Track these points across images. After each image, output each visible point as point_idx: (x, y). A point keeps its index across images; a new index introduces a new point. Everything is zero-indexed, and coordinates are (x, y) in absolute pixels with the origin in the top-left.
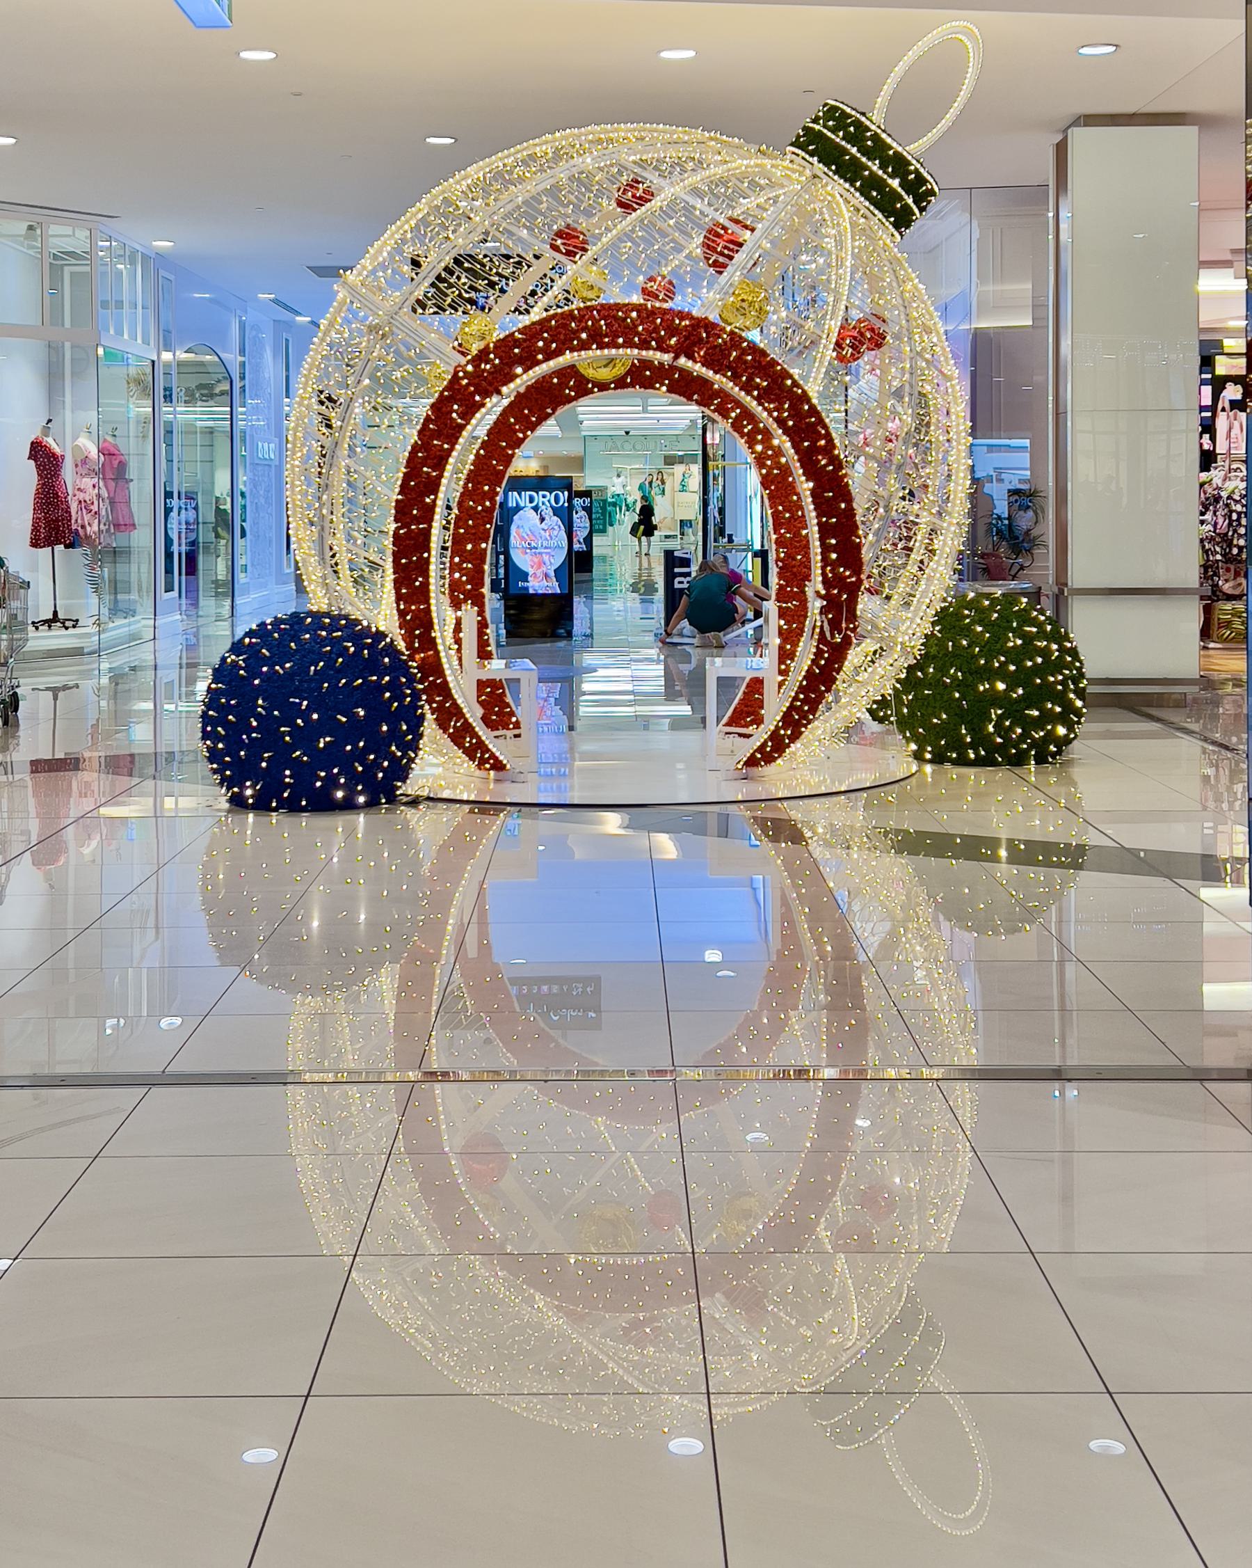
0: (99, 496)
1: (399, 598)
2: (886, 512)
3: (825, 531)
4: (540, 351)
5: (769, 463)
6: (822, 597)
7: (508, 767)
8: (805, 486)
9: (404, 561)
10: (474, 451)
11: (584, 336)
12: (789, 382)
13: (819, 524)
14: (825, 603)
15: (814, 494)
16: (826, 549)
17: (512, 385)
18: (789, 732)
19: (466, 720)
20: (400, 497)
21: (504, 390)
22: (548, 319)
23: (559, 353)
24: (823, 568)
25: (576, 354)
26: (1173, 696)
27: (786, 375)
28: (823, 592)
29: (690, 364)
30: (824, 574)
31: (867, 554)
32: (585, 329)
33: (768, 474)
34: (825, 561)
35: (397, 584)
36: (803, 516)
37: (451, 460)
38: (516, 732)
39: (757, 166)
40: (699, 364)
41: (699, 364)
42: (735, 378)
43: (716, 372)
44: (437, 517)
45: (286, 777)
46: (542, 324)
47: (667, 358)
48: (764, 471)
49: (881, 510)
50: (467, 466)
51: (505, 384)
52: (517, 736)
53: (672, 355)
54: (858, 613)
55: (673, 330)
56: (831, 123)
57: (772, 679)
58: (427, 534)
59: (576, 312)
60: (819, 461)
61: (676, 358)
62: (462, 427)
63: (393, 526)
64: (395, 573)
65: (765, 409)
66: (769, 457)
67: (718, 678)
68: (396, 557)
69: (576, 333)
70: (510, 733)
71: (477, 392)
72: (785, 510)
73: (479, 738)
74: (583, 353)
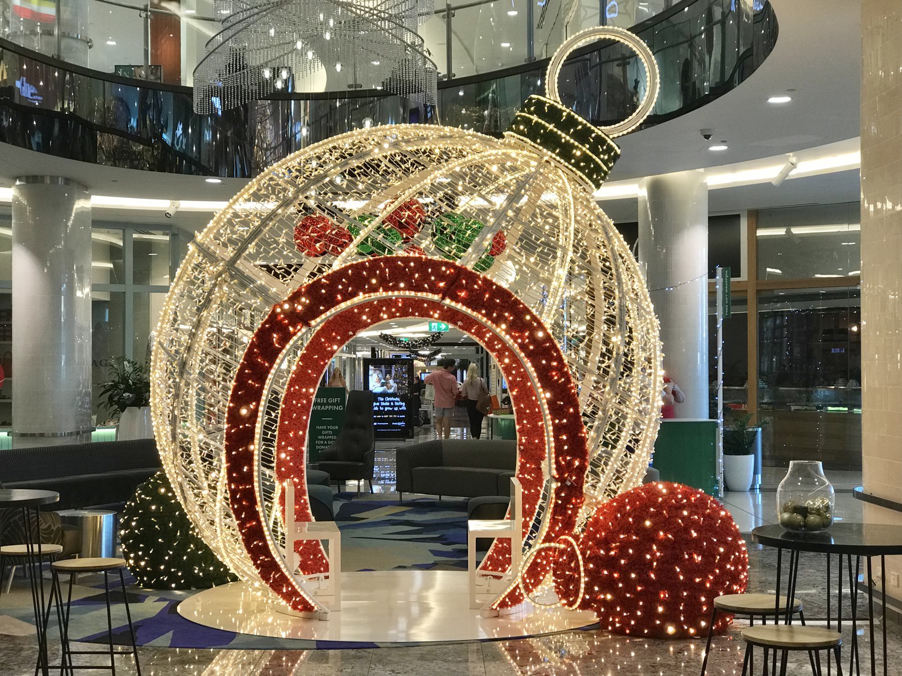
0: (163, 323)
1: (231, 479)
2: (604, 414)
3: (558, 430)
4: (340, 292)
5: (514, 372)
6: (557, 480)
7: (316, 608)
8: (544, 396)
9: (234, 453)
10: (296, 363)
11: (374, 281)
12: (528, 317)
13: (554, 424)
14: (559, 484)
15: (551, 403)
16: (559, 443)
17: (318, 320)
18: (532, 581)
19: (282, 573)
20: (231, 405)
21: (313, 323)
22: (346, 269)
23: (354, 295)
24: (557, 458)
25: (367, 295)
26: (767, 454)
27: (527, 311)
28: (557, 476)
29: (453, 304)
30: (557, 463)
31: (589, 446)
32: (375, 276)
33: (514, 380)
34: (559, 452)
35: (230, 471)
36: (540, 412)
37: (270, 376)
38: (327, 574)
39: (504, 154)
40: (460, 304)
41: (460, 304)
42: (488, 315)
43: (473, 310)
44: (259, 419)
45: (446, 271)
46: (342, 273)
47: (436, 297)
48: (510, 378)
49: (600, 413)
50: (290, 375)
51: (314, 317)
52: (327, 577)
53: (441, 295)
54: (584, 491)
55: (441, 277)
56: (532, 109)
57: (518, 543)
58: (252, 431)
59: (367, 264)
60: (553, 377)
61: (443, 298)
62: (280, 350)
63: (226, 426)
64: (227, 462)
65: (512, 337)
66: (514, 368)
67: (477, 539)
68: (229, 449)
69: (367, 280)
70: (322, 575)
71: (289, 324)
72: (526, 407)
73: (293, 587)
74: (372, 294)
